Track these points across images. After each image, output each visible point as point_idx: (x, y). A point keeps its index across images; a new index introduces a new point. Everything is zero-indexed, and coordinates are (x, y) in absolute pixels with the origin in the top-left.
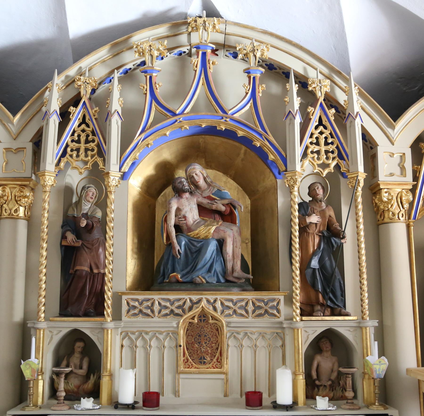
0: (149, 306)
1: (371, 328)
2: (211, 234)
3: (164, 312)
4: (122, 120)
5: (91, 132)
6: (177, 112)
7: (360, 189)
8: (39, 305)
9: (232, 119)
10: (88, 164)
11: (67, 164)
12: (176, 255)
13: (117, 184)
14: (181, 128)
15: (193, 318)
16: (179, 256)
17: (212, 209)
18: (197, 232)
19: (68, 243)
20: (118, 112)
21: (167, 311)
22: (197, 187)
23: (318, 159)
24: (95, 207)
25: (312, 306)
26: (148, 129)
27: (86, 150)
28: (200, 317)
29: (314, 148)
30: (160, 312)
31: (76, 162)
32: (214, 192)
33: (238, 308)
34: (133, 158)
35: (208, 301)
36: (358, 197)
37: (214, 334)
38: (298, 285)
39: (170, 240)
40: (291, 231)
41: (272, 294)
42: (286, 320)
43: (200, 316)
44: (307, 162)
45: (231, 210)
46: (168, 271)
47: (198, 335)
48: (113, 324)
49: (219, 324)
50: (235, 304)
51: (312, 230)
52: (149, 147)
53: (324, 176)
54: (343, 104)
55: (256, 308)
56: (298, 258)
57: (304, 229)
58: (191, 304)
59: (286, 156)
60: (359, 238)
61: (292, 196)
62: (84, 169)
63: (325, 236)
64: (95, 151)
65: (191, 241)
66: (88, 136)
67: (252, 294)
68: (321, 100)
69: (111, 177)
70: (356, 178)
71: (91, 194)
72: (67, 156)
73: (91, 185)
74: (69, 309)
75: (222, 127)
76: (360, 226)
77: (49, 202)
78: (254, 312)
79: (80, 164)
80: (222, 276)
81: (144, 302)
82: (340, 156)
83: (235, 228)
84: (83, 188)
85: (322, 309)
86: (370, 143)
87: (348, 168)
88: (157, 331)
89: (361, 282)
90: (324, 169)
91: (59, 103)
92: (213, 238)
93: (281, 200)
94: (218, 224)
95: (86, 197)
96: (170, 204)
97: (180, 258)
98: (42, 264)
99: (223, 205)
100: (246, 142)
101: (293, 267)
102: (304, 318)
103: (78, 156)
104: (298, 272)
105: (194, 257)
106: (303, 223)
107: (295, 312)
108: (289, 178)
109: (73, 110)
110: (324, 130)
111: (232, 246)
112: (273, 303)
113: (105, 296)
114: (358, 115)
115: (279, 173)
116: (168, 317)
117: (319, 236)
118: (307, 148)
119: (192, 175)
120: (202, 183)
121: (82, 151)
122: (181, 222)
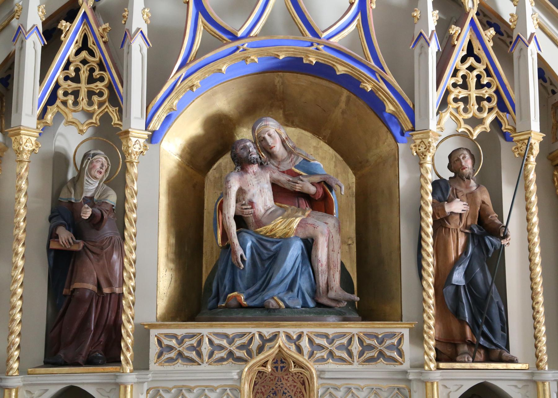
0: (194, 346)
1: (551, 383)
2: (293, 231)
3: (218, 355)
4: (149, 45)
5: (98, 64)
6: (240, 34)
7: (532, 159)
8: (9, 348)
9: (327, 47)
10: (94, 118)
11: (58, 116)
12: (238, 263)
13: (141, 150)
14: (245, 59)
15: (264, 365)
16: (242, 266)
17: (295, 191)
18: (270, 226)
19: (61, 245)
20: (141, 32)
21: (223, 354)
22: (271, 155)
23: (466, 110)
24: (105, 186)
25: (455, 346)
26: (191, 62)
27: (90, 93)
28: (275, 363)
29: (459, 92)
30: (211, 355)
31: (74, 113)
32: (297, 163)
33: (337, 348)
34: (167, 107)
35: (288, 337)
36: (529, 173)
37: (299, 390)
38: (431, 312)
39: (227, 239)
40: (421, 226)
41: (390, 326)
42: (413, 367)
43: (275, 362)
44: (446, 116)
45: (325, 192)
46: (225, 288)
47: (273, 392)
48: (134, 376)
49: (307, 374)
50: (331, 342)
51: (454, 224)
52: (194, 90)
53: (475, 137)
54: (508, 21)
56: (431, 269)
57: (441, 222)
58: (261, 343)
59: (414, 106)
60: (531, 237)
61: (422, 170)
62: (87, 125)
63: (476, 234)
64: (105, 96)
65: (261, 241)
66: (92, 70)
67: (358, 326)
68: (473, 14)
69: (132, 138)
70: (526, 141)
71: (98, 166)
72: (58, 102)
73: (99, 152)
74: (61, 354)
75: (311, 59)
76: (532, 219)
77: (27, 179)
78: (361, 354)
79: (79, 117)
80: (310, 296)
81: (186, 340)
82: (502, 106)
83: (331, 221)
84: (86, 156)
85: (471, 350)
86: (551, 84)
87: (514, 125)
88: (207, 387)
89: (533, 308)
90: (474, 127)
91: (40, 13)
92: (296, 236)
93: (404, 177)
94: (304, 214)
95: (90, 170)
96: (228, 182)
97: (244, 269)
98: (16, 281)
99: (313, 184)
100: (350, 83)
101: (424, 283)
102: (442, 365)
103: (76, 103)
104: (431, 291)
105: (266, 266)
106: (440, 213)
107: (428, 355)
108: (418, 142)
109: (66, 27)
110: (476, 64)
111: (326, 249)
112: (393, 341)
113: (123, 331)
114: (533, 39)
115: (402, 134)
116: (224, 363)
117: (466, 233)
118: (447, 93)
119: (263, 136)
120: (278, 148)
121: (83, 94)
122: (245, 210)
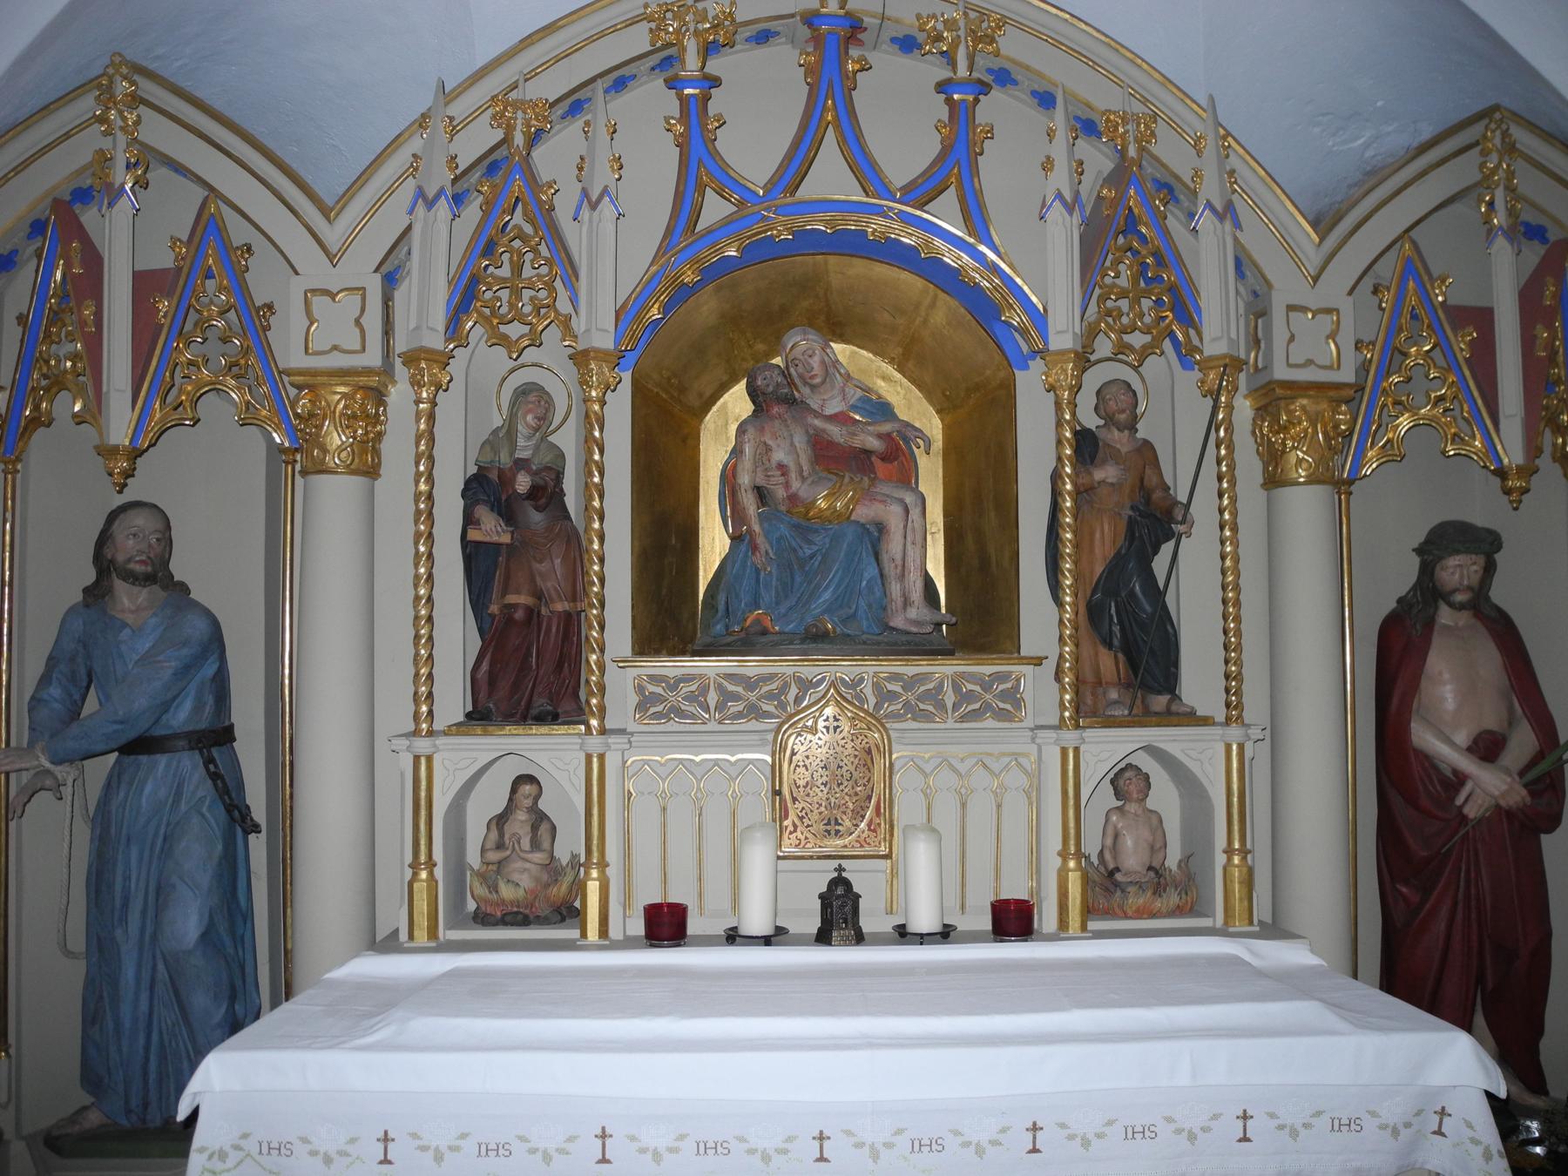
20: (313, 291)
55: (964, 698)
78: (955, 707)
